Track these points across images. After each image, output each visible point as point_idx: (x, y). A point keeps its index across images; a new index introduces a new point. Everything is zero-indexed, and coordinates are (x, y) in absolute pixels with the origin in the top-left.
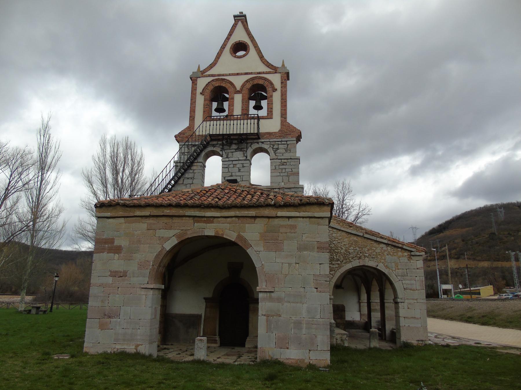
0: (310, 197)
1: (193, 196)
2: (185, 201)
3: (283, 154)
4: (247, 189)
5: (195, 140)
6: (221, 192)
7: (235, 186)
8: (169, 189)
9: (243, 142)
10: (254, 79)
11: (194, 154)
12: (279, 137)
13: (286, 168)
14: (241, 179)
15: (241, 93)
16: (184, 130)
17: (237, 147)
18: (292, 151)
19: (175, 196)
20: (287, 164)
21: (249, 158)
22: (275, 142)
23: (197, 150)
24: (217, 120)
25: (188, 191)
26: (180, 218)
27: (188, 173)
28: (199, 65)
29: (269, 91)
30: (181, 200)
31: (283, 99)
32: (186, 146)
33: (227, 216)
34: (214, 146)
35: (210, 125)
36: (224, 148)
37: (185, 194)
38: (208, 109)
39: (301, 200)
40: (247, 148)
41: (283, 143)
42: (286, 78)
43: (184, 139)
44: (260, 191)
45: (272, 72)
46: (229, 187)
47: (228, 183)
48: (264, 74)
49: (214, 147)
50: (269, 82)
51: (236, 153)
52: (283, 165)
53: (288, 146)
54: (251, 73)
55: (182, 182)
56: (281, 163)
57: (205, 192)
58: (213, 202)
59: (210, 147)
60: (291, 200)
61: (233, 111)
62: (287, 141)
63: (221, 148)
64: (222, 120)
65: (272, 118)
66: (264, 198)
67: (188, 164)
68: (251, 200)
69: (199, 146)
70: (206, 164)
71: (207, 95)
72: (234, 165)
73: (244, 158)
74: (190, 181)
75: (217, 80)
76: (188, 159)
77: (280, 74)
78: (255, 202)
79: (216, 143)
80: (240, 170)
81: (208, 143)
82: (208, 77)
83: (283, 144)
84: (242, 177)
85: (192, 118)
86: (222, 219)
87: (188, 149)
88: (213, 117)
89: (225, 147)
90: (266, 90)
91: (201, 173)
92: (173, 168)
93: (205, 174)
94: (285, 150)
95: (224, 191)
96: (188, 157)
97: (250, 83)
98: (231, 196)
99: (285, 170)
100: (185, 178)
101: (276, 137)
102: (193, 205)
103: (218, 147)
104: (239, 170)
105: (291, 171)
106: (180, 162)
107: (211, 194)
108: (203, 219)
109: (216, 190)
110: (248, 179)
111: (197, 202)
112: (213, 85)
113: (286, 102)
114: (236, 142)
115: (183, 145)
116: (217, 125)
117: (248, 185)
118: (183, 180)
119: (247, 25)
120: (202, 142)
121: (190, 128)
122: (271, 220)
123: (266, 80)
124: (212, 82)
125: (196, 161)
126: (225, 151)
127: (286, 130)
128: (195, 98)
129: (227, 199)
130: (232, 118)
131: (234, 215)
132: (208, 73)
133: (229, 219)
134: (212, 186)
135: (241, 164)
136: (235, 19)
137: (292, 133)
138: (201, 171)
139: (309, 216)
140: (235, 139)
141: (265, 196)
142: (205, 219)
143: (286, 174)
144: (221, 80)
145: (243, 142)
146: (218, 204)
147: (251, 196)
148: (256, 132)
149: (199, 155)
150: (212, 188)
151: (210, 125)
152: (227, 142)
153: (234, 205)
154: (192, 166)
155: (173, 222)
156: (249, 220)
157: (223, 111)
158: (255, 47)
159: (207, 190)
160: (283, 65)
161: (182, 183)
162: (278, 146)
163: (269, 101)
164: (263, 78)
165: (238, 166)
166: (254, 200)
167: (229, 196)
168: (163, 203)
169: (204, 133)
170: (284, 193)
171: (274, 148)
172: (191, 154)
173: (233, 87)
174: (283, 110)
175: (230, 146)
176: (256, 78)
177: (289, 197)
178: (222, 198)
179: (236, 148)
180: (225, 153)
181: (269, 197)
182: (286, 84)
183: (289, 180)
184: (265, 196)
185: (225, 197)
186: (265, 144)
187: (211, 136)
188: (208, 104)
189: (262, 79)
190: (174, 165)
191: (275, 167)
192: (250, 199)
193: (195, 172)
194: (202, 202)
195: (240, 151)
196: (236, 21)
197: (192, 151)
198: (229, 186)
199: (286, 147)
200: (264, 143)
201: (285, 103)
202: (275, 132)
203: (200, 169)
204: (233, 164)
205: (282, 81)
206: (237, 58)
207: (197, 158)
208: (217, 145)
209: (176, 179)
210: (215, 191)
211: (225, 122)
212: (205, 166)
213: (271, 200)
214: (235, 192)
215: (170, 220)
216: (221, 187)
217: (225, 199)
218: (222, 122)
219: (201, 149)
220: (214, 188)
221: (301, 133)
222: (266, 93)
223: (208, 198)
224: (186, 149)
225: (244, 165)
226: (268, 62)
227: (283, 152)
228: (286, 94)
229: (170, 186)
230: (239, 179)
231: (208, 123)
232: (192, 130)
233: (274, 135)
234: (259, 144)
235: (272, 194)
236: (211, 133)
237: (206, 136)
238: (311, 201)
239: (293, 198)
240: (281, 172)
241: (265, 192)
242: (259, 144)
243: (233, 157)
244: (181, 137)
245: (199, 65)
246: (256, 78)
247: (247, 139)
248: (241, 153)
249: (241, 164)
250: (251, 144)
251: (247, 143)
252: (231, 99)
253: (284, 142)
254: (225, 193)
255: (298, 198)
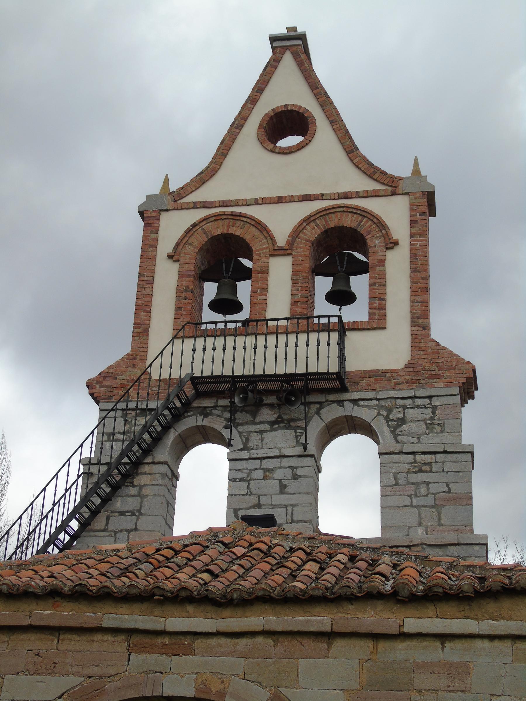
0: (511, 569)
1: (130, 566)
2: (103, 579)
3: (419, 439)
4: (305, 545)
5: (148, 394)
6: (221, 553)
7: (266, 534)
8: (61, 546)
9: (293, 399)
10: (328, 212)
11: (144, 436)
12: (406, 385)
13: (430, 481)
14: (289, 517)
15: (291, 254)
16: (117, 365)
17: (276, 416)
18: (447, 429)
19: (73, 565)
20: (434, 470)
21: (312, 449)
22: (393, 401)
23: (152, 426)
24: (214, 334)
25: (118, 550)
26: (85, 637)
27: (122, 497)
28: (167, 175)
29: (375, 246)
30: (92, 577)
31: (416, 271)
32: (119, 413)
33: (237, 630)
34: (205, 412)
35: (194, 350)
36: (235, 419)
37: (106, 560)
38: (191, 301)
39: (482, 580)
40: (307, 420)
41: (419, 402)
42: (425, 209)
43: (115, 391)
44: (346, 550)
45: (381, 193)
46: (248, 537)
47: (245, 524)
48: (359, 197)
49: (207, 417)
50: (375, 220)
51: (274, 433)
52: (421, 471)
53: (434, 413)
54: (320, 197)
55: (104, 523)
56: (415, 466)
57: (169, 553)
58: (193, 584)
59: (195, 417)
60: (450, 578)
61: (265, 308)
62: (430, 397)
63: (226, 419)
64: (230, 335)
65: (385, 328)
66: (361, 573)
67: (123, 469)
68: (317, 579)
69: (160, 412)
70: (179, 471)
71: (188, 261)
72: (265, 470)
73: (299, 450)
74: (128, 522)
75: (218, 217)
76: (124, 453)
77: (406, 198)
78: (329, 585)
79: (213, 405)
80: (285, 486)
81: (187, 405)
82: (193, 208)
83: (420, 407)
84: (290, 509)
85: (140, 330)
86: (223, 641)
87: (125, 421)
88: (203, 327)
89: (238, 415)
90: (368, 254)
91: (164, 496)
92: (77, 480)
93: (175, 499)
94: (426, 424)
95: (232, 550)
96: (124, 447)
97: (317, 225)
98: (253, 565)
99: (428, 488)
100: (112, 512)
101: (395, 383)
102: (128, 593)
103: (218, 416)
104: (283, 488)
105: (446, 489)
106: (99, 463)
107: (188, 559)
108: (160, 640)
109: (207, 547)
110: (308, 517)
111: (142, 584)
112: (205, 233)
113: (426, 278)
114: (272, 399)
115: (110, 411)
116: (214, 349)
117: (309, 533)
118: (108, 518)
119: (307, 61)
120: (168, 400)
121: (135, 358)
122: (382, 645)
123: (364, 217)
124: (204, 223)
125: (149, 459)
126: (240, 428)
127: (427, 365)
128: (153, 271)
129: (240, 576)
130: (262, 328)
131: (260, 628)
132: (192, 198)
133: (243, 642)
134: (193, 535)
135: (288, 469)
136: (274, 45)
137: (447, 373)
138: (163, 491)
139: (512, 632)
140: (270, 392)
141: (362, 564)
142: (167, 640)
143: (430, 500)
144: (230, 217)
145: (293, 399)
146: (207, 590)
147: (319, 565)
148: (334, 368)
149: (157, 440)
150: (192, 541)
151: (194, 350)
152: (244, 399)
153: (260, 594)
154: (137, 474)
155: (60, 648)
156: (310, 644)
157: (237, 307)
158: (332, 122)
159: (178, 547)
160: (416, 171)
161: (103, 528)
162: (404, 413)
163: (375, 277)
164: (355, 211)
165: (279, 474)
166: (326, 577)
167: (247, 565)
168: (31, 585)
169: (175, 375)
170: (426, 557)
171: (391, 417)
172: (135, 436)
173: (266, 238)
174: (417, 302)
175: (254, 415)
176: (334, 210)
177: (440, 569)
178: (223, 571)
179: (273, 419)
180: (240, 433)
181: (378, 569)
182: (425, 227)
183: (439, 519)
184: (362, 564)
185: (235, 568)
186: (362, 406)
187: (195, 380)
188: (191, 287)
189: (352, 212)
190: (81, 471)
191: (395, 478)
192: (314, 576)
193: (143, 492)
194: (158, 584)
195: (286, 428)
196: (278, 51)
197: (138, 428)
198: (249, 536)
199: (427, 417)
200: (361, 403)
201: (424, 281)
202: (393, 371)
203: (160, 485)
204: (262, 469)
205: (413, 218)
206: (279, 153)
207: (151, 451)
208: (214, 411)
209: (87, 515)
210: (203, 551)
211: (240, 340)
212: (176, 477)
213: (384, 579)
214: (267, 554)
215: (53, 641)
216: (222, 539)
217: (231, 576)
218: (230, 341)
219: (164, 423)
220: (199, 540)
221: (474, 371)
222: (365, 254)
223: (177, 572)
224: (120, 421)
225: (299, 472)
226: (370, 164)
227: (421, 432)
228: (425, 256)
229: (63, 537)
230: (280, 516)
231: (189, 343)
232: (139, 365)
233: (389, 379)
234: (343, 406)
235: (386, 559)
236: (197, 373)
237: (180, 382)
238: (517, 582)
239: (456, 573)
240: (413, 493)
241: (364, 555)
242: (343, 406)
243: (262, 448)
244: (106, 387)
245: (167, 175)
246: (334, 210)
247: (307, 391)
248: (290, 433)
249: (289, 467)
250: (318, 406)
251: (307, 404)
252: (260, 272)
253: (421, 400)
254: (235, 557)
255: (471, 574)
